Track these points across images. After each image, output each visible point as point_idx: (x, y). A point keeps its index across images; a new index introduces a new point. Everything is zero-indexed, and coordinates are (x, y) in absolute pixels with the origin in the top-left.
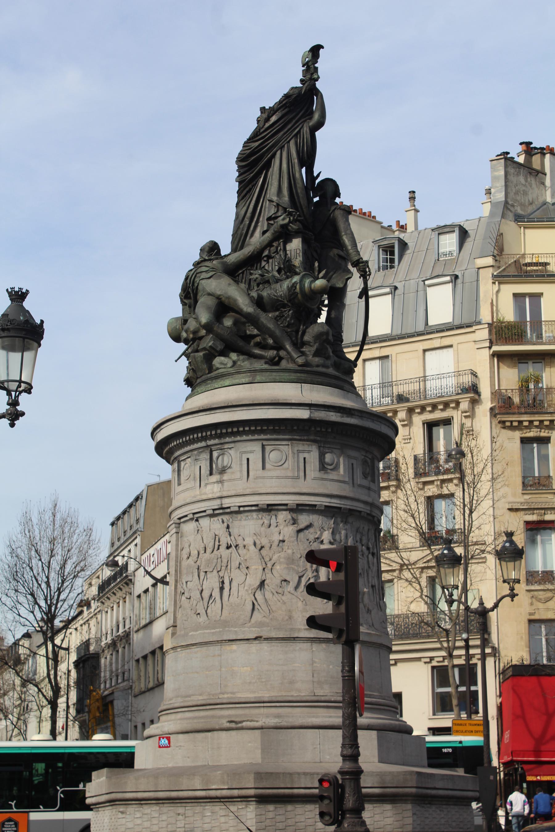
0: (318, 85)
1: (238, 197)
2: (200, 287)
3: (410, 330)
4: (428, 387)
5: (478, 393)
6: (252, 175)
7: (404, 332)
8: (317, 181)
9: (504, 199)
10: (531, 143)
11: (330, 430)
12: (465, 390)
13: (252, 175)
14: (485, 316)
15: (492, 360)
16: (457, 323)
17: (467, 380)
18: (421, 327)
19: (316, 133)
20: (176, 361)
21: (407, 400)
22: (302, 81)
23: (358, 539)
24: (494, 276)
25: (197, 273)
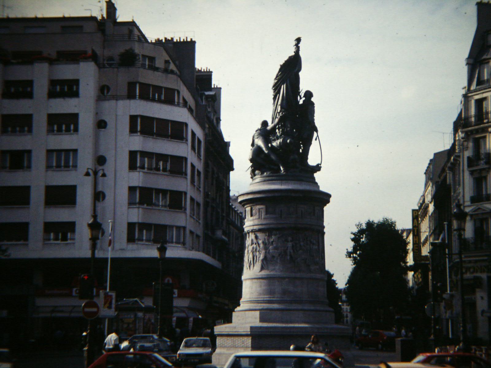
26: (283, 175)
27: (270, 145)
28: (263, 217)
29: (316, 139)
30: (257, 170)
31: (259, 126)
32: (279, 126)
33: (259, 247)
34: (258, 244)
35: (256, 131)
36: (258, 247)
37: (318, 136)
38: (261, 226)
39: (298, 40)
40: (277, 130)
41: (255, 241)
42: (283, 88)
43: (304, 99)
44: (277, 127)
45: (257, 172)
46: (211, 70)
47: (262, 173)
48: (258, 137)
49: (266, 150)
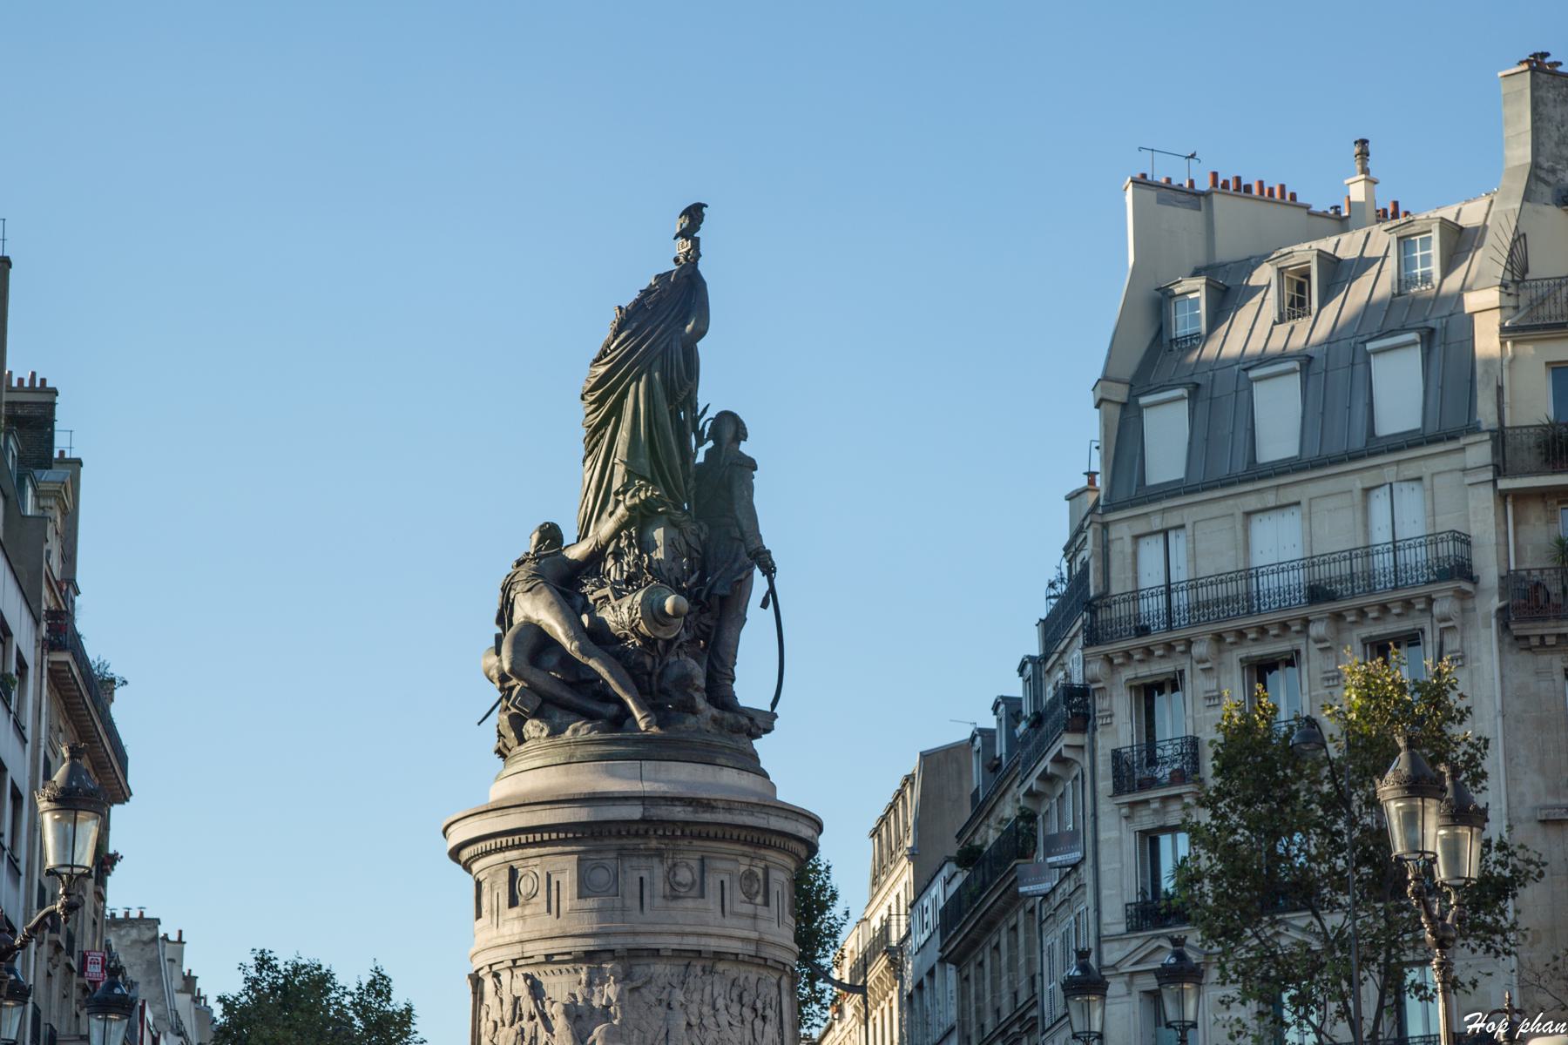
3: (1335, 448)
4: (1401, 561)
5: (1472, 579)
7: (1325, 453)
9: (1529, 160)
10: (1547, 55)
11: (678, 833)
12: (1444, 575)
14: (1486, 412)
15: (1501, 507)
16: (1432, 429)
17: (1447, 549)
18: (1358, 443)
21: (1331, 597)
23: (735, 996)
24: (1503, 329)
26: (648, 739)
27: (585, 619)
28: (565, 905)
29: (764, 605)
32: (618, 544)
33: (549, 1029)
34: (544, 1017)
35: (520, 563)
36: (541, 1029)
37: (772, 590)
38: (591, 941)
39: (695, 214)
40: (610, 563)
41: (527, 1005)
42: (635, 397)
43: (710, 444)
46: (49, 385)
47: (555, 732)
48: (529, 586)
49: (572, 639)
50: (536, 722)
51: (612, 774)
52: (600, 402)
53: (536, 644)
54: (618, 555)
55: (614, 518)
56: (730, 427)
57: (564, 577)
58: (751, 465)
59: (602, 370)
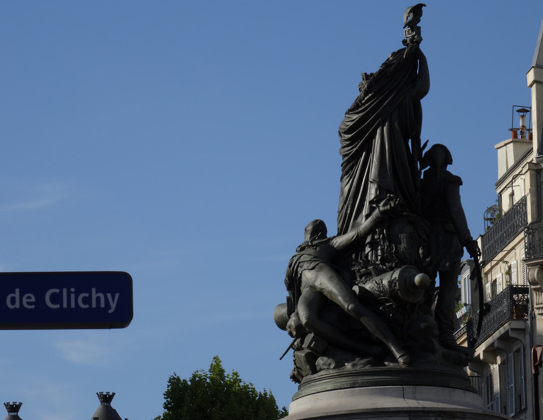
0: (423, 47)
1: (343, 170)
2: (303, 279)
6: (355, 149)
8: (424, 152)
13: (355, 149)
19: (421, 101)
20: (281, 359)
22: (166, 407)
25: (299, 263)
30: (323, 355)
31: (304, 238)
32: (373, 237)
40: (368, 249)
44: (368, 239)
45: (321, 361)
47: (339, 365)
50: (325, 358)
51: (384, 394)
52: (352, 141)
53: (321, 302)
54: (374, 245)
55: (370, 219)
56: (441, 155)
57: (340, 261)
58: (458, 181)
59: (355, 117)
